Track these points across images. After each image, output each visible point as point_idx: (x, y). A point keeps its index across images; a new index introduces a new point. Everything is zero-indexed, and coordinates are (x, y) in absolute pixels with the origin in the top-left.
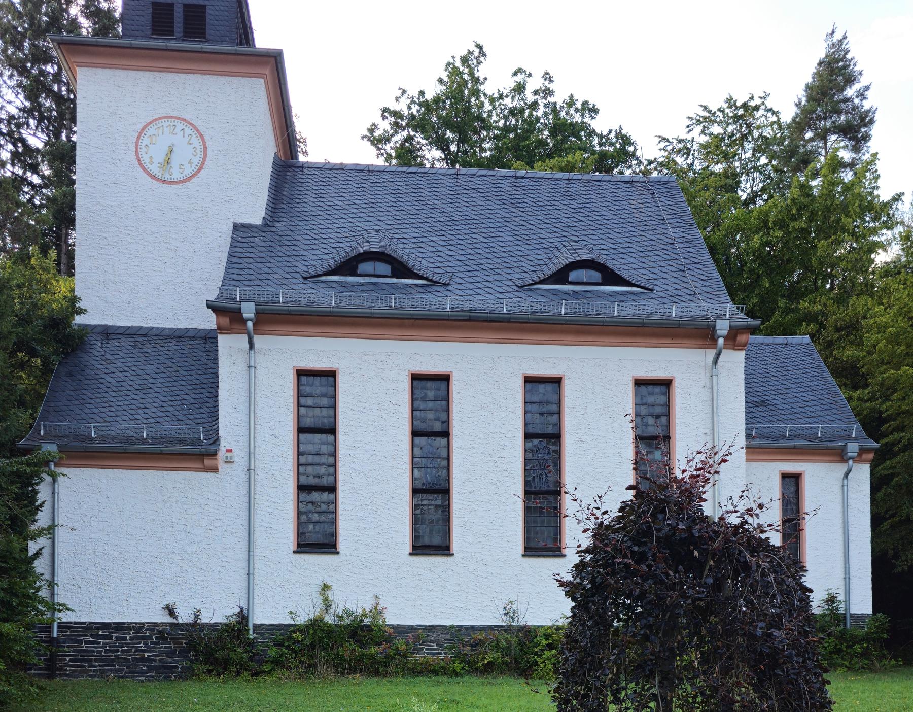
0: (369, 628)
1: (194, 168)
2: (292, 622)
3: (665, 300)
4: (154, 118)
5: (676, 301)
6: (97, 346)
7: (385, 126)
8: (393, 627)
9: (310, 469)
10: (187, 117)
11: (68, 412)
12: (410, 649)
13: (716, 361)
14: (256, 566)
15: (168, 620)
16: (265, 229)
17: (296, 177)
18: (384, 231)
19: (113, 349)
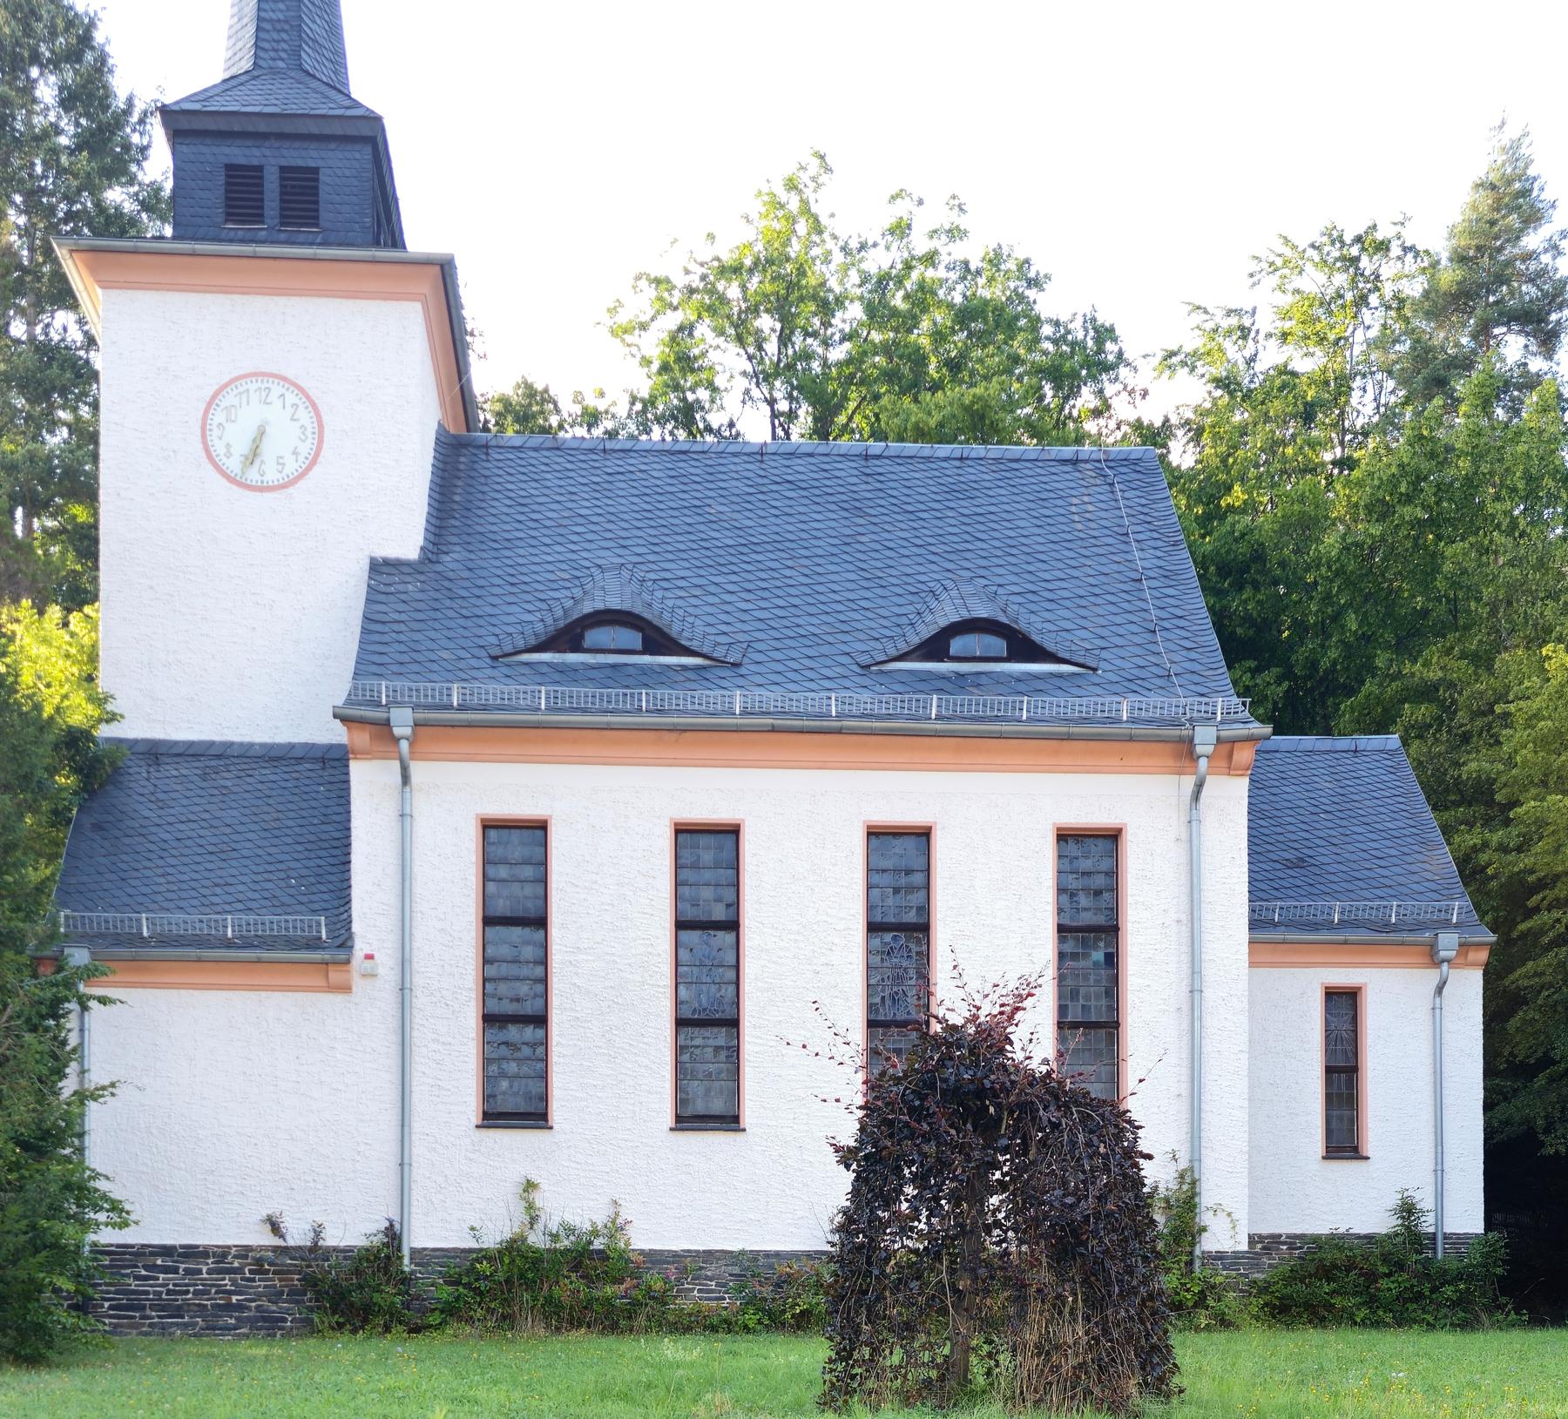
0: (602, 1255)
1: (302, 463)
2: (474, 1245)
3: (1117, 688)
5: (1135, 688)
6: (139, 775)
7: (641, 303)
8: (642, 1252)
9: (503, 988)
10: (290, 375)
11: (101, 894)
13: (1196, 796)
14: (415, 1151)
16: (426, 569)
17: (476, 466)
19: (167, 781)
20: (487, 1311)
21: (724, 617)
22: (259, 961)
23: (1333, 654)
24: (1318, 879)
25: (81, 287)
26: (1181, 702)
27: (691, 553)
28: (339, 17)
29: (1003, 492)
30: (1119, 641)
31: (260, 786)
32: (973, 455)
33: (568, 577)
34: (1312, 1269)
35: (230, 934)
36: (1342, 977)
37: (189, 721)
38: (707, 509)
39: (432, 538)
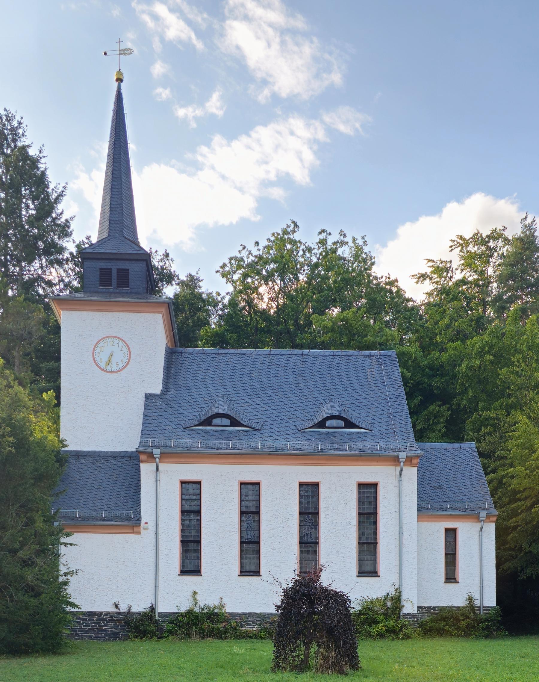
1: (124, 364)
2: (177, 611)
4: (103, 337)
8: (229, 614)
12: (238, 625)
14: (159, 582)
15: (116, 610)
16: (162, 397)
17: (178, 360)
18: (227, 396)
19: (82, 464)
20: (182, 632)
21: (256, 413)
22: (112, 525)
23: (465, 402)
24: (444, 493)
25: (55, 308)
26: (396, 443)
27: (246, 390)
28: (137, 235)
30: (380, 421)
32: (337, 354)
33: (207, 399)
34: (439, 618)
36: (451, 525)
37: (88, 445)
38: (251, 375)
39: (164, 386)
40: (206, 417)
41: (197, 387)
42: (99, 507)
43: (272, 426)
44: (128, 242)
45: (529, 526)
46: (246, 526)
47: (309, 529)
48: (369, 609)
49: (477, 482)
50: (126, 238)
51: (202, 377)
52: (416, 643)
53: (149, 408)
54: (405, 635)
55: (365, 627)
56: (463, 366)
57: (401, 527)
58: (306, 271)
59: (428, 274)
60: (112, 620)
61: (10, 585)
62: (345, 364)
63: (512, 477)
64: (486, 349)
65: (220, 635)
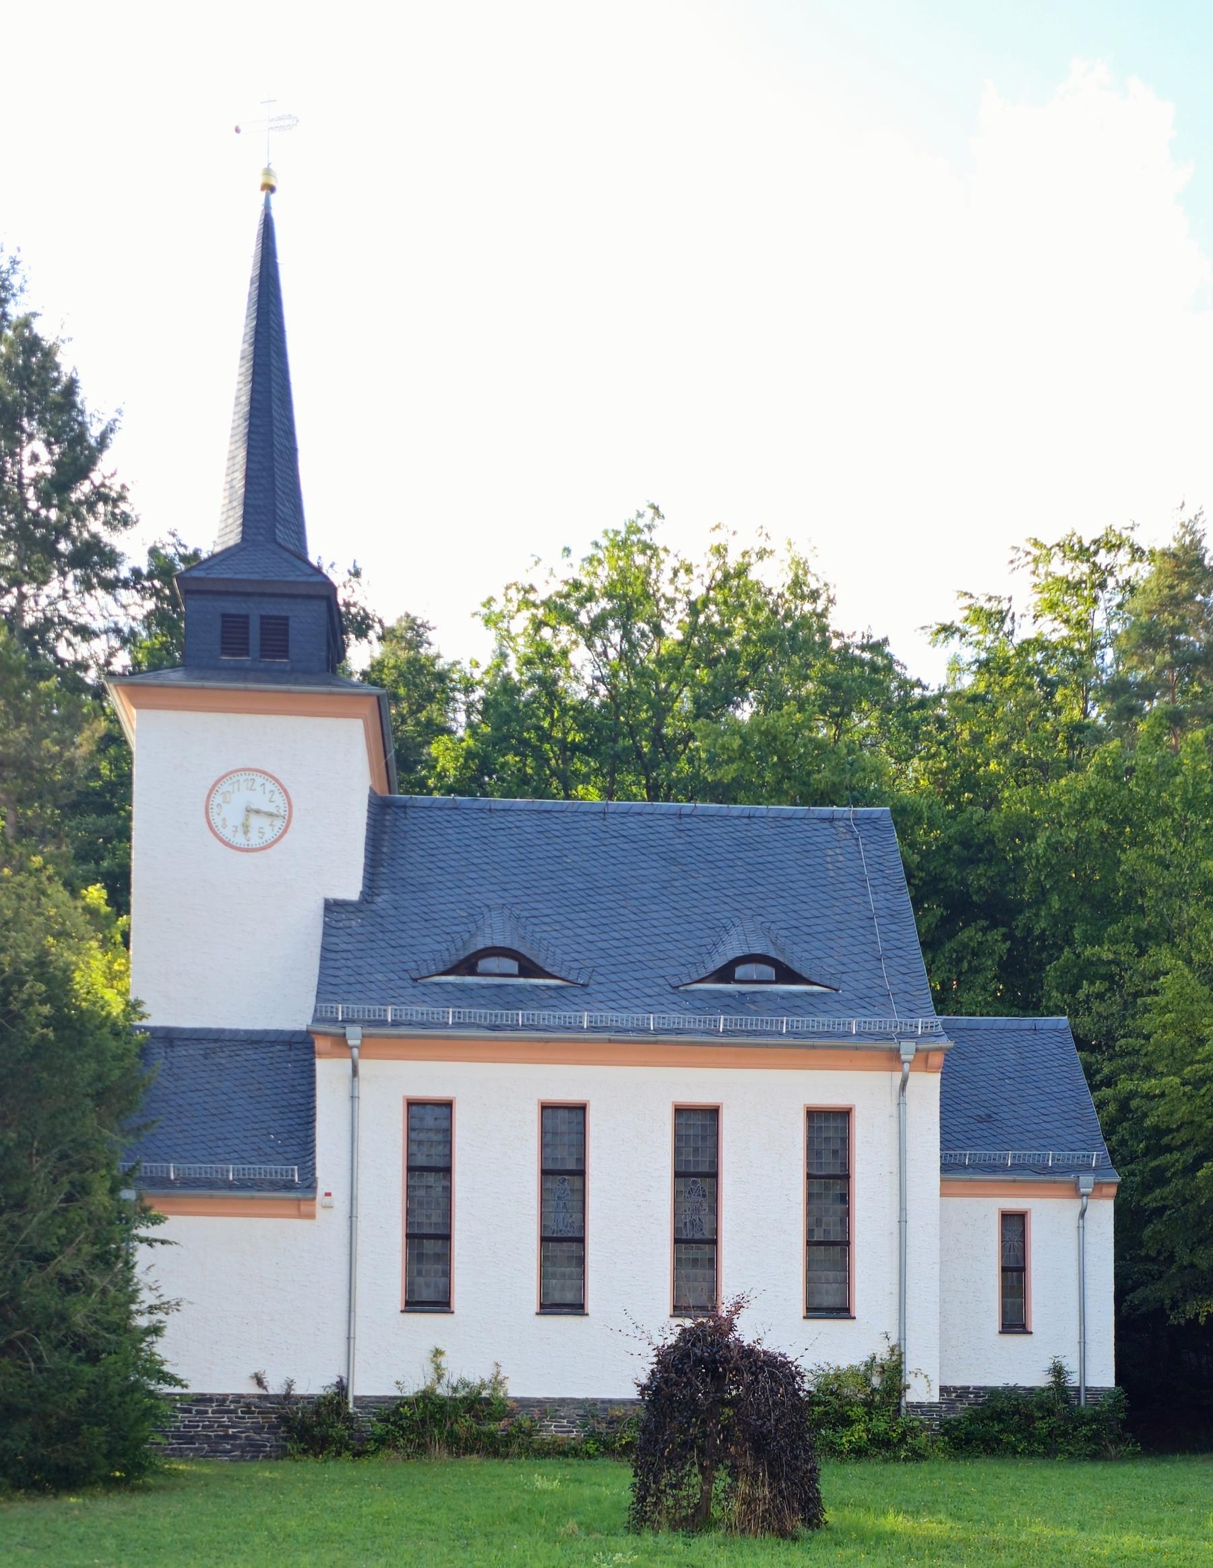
0: (488, 1402)
2: (398, 1394)
8: (516, 1400)
10: (268, 769)
15: (255, 1390)
16: (363, 908)
23: (1043, 924)
26: (895, 1021)
29: (778, 844)
30: (855, 967)
31: (245, 1063)
32: (757, 814)
34: (988, 1412)
35: (231, 1177)
36: (1014, 1204)
40: (463, 955)
41: (441, 886)
42: (221, 1157)
43: (613, 977)
44: (286, 555)
45: (1192, 1207)
46: (554, 1203)
47: (697, 1210)
48: (832, 1393)
49: (1072, 1107)
50: (280, 546)
51: (453, 863)
52: (939, 1470)
53: (334, 931)
54: (914, 1451)
55: (823, 1432)
56: (1039, 841)
57: (903, 1209)
58: (680, 616)
59: (958, 624)
60: (250, 1412)
61: (37, 1335)
62: (776, 837)
63: (1149, 1097)
64: (1091, 805)
65: (496, 1448)
